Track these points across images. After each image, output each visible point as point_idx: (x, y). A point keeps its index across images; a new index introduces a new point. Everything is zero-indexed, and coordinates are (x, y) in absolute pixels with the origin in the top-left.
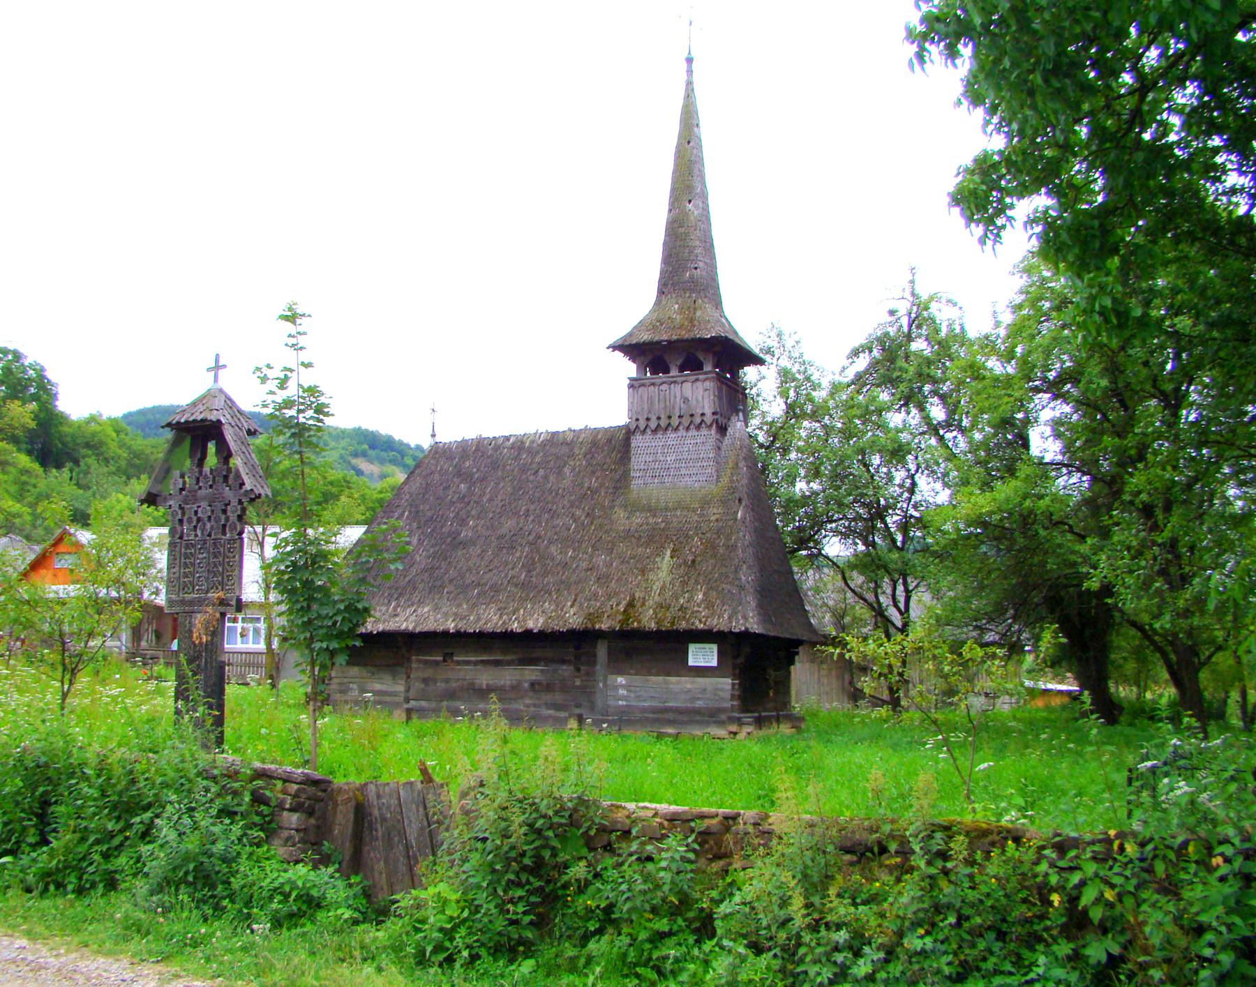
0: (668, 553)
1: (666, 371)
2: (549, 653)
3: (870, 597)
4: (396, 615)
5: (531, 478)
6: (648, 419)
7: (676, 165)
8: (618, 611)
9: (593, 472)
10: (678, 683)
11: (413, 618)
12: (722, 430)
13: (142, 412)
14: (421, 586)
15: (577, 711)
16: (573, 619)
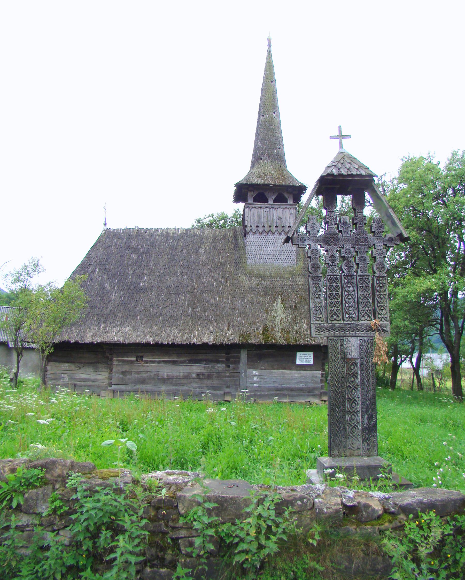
0: (280, 301)
1: (266, 201)
2: (209, 356)
9: (219, 254)
10: (290, 373)
14: (120, 315)
16: (231, 337)
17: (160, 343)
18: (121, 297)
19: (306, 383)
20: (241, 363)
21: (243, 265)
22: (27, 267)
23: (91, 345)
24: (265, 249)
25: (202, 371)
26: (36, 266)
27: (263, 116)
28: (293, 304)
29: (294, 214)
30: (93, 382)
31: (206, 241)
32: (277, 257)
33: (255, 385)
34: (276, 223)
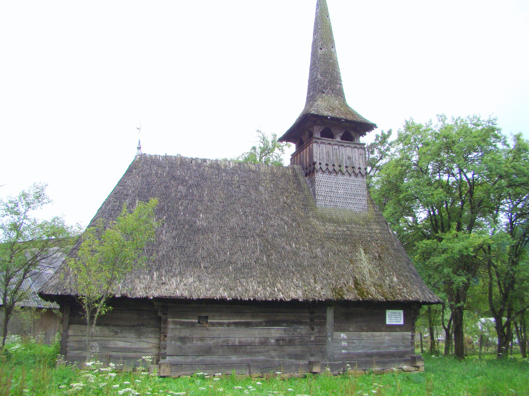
0: (362, 251)
1: (332, 136)
2: (291, 317)
6: (327, 165)
9: (282, 193)
10: (381, 336)
16: (322, 292)
17: (239, 298)
18: (174, 238)
19: (397, 346)
20: (327, 324)
21: (313, 208)
22: (25, 195)
23: (145, 301)
24: (336, 191)
25: (282, 335)
26: (39, 197)
27: (321, 49)
28: (377, 255)
30: (135, 352)
31: (264, 178)
32: (347, 201)
33: (343, 351)
34: (346, 163)
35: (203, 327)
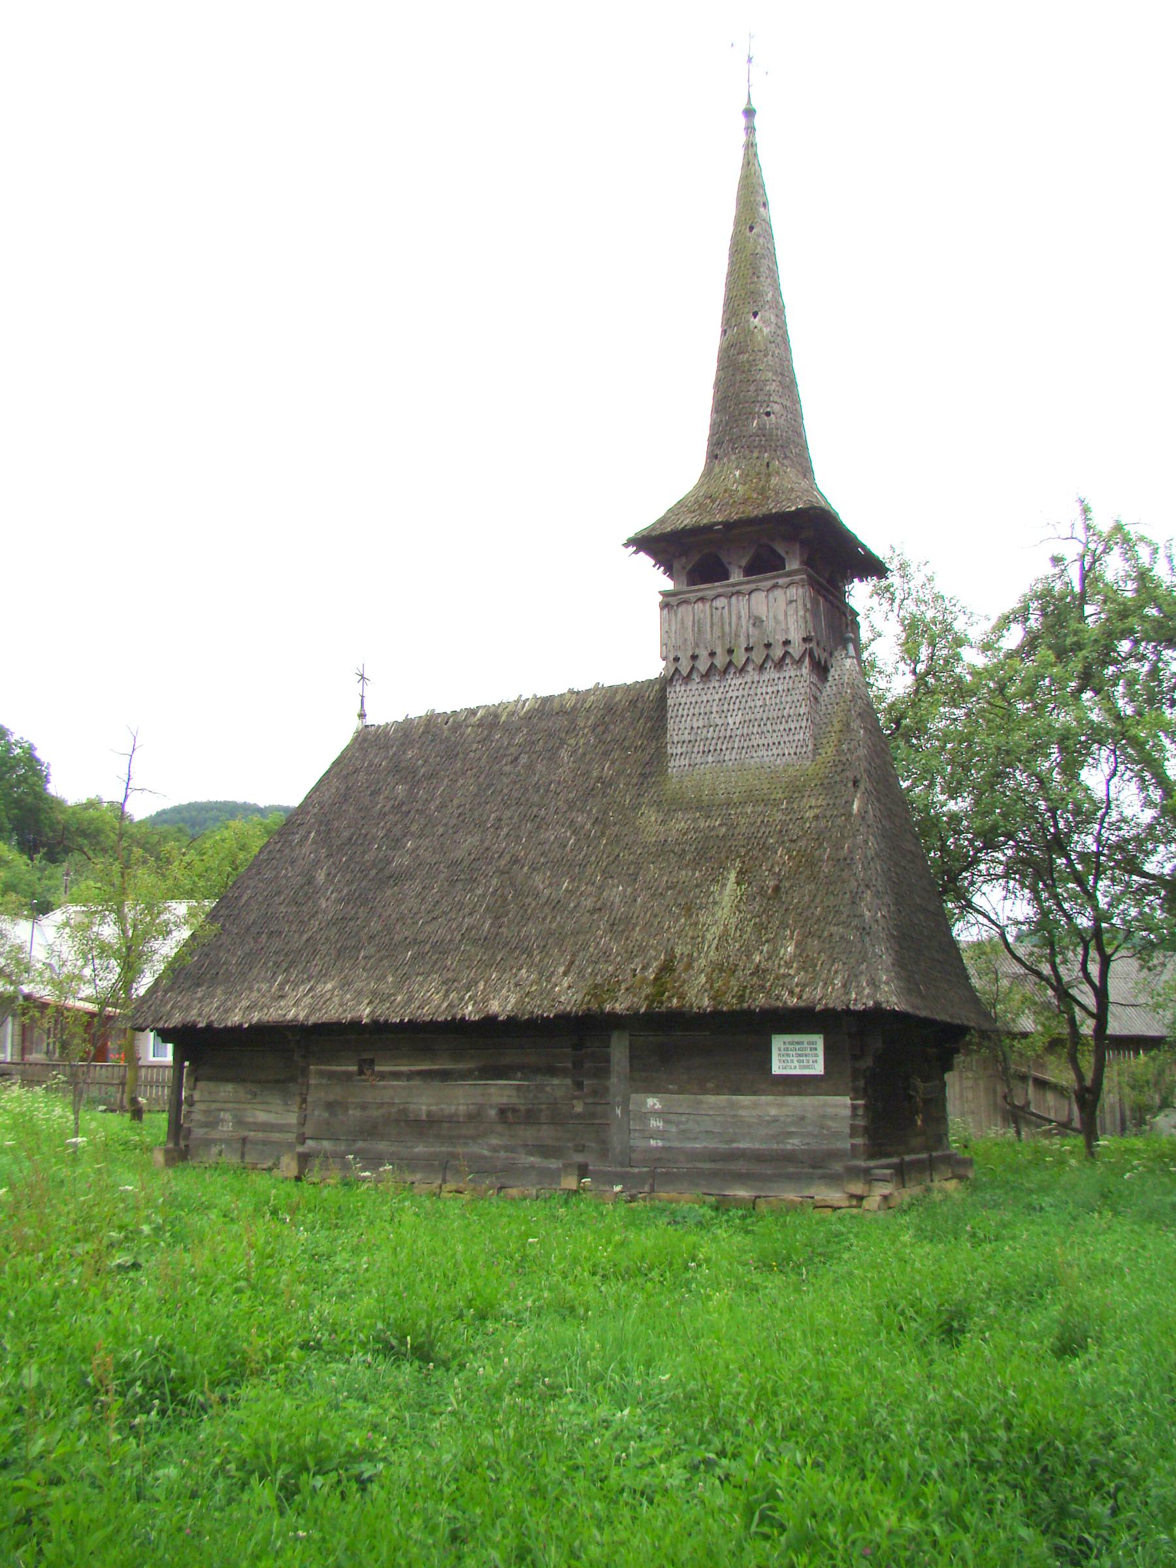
0: (732, 876)
3: (1046, 969)
4: (282, 997)
5: (508, 769)
6: (694, 657)
7: (732, 264)
8: (644, 979)
9: (606, 753)
10: (755, 1105)
11: (307, 1000)
12: (821, 670)
13: (177, 810)
14: (323, 949)
15: (579, 1158)
16: (566, 994)
29: (800, 602)
30: (281, 1131)
35: (364, 1081)
